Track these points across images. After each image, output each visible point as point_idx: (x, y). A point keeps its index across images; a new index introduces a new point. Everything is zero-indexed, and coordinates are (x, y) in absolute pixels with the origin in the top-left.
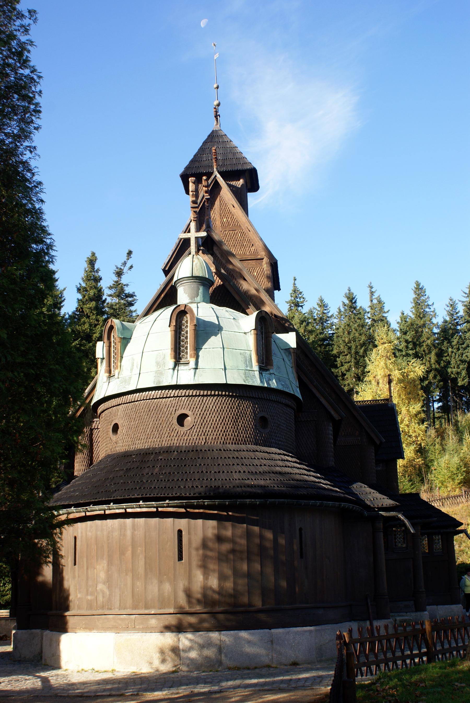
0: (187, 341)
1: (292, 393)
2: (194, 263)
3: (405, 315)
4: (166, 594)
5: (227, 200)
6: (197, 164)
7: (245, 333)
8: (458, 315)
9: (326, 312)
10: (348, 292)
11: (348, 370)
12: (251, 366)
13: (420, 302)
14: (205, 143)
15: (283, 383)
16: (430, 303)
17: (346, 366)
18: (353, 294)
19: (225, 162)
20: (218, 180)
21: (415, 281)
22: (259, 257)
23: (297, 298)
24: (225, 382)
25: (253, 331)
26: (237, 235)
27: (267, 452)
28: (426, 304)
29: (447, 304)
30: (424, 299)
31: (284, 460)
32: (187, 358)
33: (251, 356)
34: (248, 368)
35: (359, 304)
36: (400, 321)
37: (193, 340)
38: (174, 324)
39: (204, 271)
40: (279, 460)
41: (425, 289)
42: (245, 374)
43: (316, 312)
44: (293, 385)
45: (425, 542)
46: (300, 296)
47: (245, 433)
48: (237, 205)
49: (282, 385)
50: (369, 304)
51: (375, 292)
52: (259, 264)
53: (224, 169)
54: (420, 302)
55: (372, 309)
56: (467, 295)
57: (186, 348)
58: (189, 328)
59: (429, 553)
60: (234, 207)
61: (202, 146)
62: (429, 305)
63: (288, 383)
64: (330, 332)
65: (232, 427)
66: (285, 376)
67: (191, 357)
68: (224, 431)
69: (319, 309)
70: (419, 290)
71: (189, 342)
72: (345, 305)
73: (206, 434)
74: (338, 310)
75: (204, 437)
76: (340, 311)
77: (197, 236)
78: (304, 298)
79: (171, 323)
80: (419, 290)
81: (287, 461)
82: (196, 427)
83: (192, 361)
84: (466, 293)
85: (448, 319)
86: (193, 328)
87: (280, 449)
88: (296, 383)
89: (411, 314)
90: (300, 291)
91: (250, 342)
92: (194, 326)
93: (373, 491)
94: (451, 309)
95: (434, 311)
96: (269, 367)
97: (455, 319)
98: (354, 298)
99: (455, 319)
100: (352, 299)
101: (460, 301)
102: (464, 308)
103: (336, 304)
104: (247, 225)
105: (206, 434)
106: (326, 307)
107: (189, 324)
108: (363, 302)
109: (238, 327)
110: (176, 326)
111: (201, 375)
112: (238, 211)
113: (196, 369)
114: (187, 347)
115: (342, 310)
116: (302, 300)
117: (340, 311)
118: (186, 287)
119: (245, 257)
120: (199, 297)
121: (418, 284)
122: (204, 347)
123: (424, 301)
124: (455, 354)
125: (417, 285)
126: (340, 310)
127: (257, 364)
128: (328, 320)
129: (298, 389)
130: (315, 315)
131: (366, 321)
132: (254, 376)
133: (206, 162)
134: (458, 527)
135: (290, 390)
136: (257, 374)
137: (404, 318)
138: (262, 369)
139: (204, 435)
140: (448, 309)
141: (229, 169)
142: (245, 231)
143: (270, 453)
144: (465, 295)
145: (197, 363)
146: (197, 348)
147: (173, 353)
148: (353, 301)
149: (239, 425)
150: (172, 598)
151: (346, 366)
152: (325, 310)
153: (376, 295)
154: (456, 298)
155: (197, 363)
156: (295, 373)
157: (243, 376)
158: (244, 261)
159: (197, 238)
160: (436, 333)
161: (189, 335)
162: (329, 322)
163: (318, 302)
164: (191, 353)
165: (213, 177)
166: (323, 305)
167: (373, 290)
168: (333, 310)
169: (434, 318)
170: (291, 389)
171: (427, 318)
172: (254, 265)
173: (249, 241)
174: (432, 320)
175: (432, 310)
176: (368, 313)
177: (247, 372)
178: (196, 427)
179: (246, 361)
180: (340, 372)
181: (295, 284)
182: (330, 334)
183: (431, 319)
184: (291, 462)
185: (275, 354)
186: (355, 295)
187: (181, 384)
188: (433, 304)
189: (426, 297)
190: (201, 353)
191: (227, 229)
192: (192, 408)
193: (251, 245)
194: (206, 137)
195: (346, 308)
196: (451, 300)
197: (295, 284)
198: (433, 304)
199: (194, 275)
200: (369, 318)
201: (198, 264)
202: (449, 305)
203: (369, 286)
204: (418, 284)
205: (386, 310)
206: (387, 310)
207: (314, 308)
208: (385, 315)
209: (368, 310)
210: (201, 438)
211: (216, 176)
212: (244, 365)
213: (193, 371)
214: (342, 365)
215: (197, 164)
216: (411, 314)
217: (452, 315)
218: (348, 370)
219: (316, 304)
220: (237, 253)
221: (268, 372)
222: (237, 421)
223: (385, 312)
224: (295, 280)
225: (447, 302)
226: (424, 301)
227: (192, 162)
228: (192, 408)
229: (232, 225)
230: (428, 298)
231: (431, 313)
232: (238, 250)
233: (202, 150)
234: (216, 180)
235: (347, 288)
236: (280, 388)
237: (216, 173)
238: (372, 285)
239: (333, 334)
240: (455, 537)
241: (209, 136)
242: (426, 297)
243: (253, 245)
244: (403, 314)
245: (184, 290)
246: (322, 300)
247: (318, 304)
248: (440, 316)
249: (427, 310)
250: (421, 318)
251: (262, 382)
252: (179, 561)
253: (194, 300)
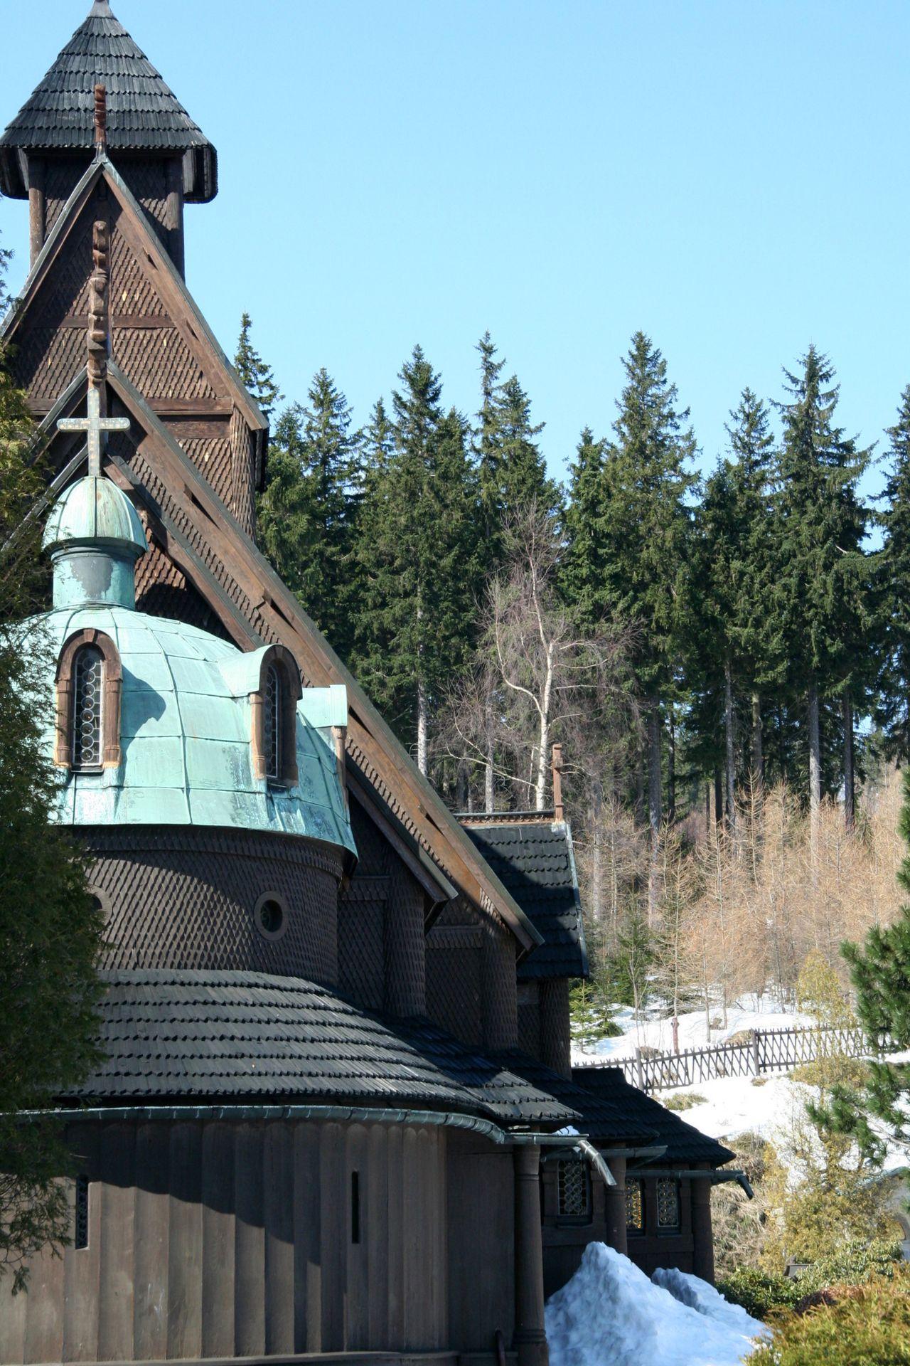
0: (98, 719)
1: (338, 842)
2: (100, 504)
3: (594, 442)
4: (46, 1327)
5: (130, 236)
6: (42, 122)
7: (233, 698)
8: (769, 449)
9: (336, 422)
10: (412, 361)
11: (402, 621)
12: (249, 782)
13: (644, 411)
14: (66, 54)
15: (319, 821)
16: (678, 408)
17: (398, 607)
18: (429, 369)
19: (127, 122)
20: (108, 179)
21: (632, 334)
22: (218, 410)
23: (252, 386)
24: (188, 822)
25: (253, 697)
26: (159, 343)
27: (279, 988)
28: (665, 411)
29: (736, 408)
30: (660, 393)
31: (320, 1008)
32: (96, 759)
33: (247, 757)
34: (242, 787)
35: (444, 405)
36: (576, 461)
37: (112, 716)
38: (68, 676)
39: (125, 527)
40: (308, 1007)
41: (665, 362)
42: (234, 800)
43: (307, 420)
44: (339, 820)
45: (636, 1201)
46: (261, 378)
47: (229, 942)
48: (160, 257)
49: (317, 825)
50: (478, 403)
51: (499, 366)
52: (219, 428)
53: (126, 142)
54: (644, 411)
55: (487, 422)
56: (798, 388)
57: (96, 734)
58: (102, 686)
59: (643, 1231)
60: (150, 260)
61: (57, 64)
62: (671, 415)
63: (329, 818)
64: (347, 491)
65: (199, 928)
66: (323, 801)
67: (108, 757)
68: (182, 938)
69: (316, 413)
70: (644, 361)
71: (101, 721)
72: (404, 405)
73: (139, 944)
74: (375, 414)
75: (134, 952)
76: (381, 418)
77: (103, 426)
78: (272, 388)
79: (62, 675)
80: (644, 361)
81: (326, 1008)
82: (116, 926)
83: (111, 769)
84: (795, 381)
85: (734, 461)
86: (114, 687)
87: (307, 979)
88: (344, 814)
89: (614, 439)
90: (262, 363)
91: (245, 722)
92: (115, 684)
93: (519, 1080)
94: (746, 426)
95: (689, 437)
96: (289, 782)
97: (757, 463)
98: (433, 383)
99: (757, 463)
100: (422, 382)
101: (776, 404)
102: (786, 427)
103: (370, 393)
104: (179, 298)
105: (139, 944)
106: (340, 407)
107: (102, 677)
108: (461, 397)
109: (217, 681)
110: (71, 681)
111: (133, 802)
112: (162, 273)
113: (119, 787)
114: (97, 733)
115: (393, 417)
116: (266, 392)
117: (381, 418)
118: (79, 562)
119: (179, 409)
120: (111, 590)
121: (642, 344)
122: (138, 734)
123: (658, 402)
124: (752, 578)
125: (638, 349)
126: (381, 411)
127: (261, 776)
128: (340, 453)
129: (349, 830)
130: (302, 433)
131: (467, 459)
132: (255, 805)
133: (71, 117)
134: (721, 1165)
135: (334, 838)
136: (261, 800)
137: (589, 452)
138: (274, 788)
139: (135, 946)
140: (735, 426)
141: (139, 142)
142: (183, 333)
143: (286, 990)
144: (792, 386)
145: (121, 774)
146: (122, 738)
147: (64, 747)
148: (430, 395)
149: (215, 923)
150: (59, 1335)
151: (398, 607)
152: (335, 416)
153: (503, 377)
154: (762, 395)
155: (121, 774)
156: (342, 788)
157: (230, 806)
158: (181, 425)
159: (102, 433)
160: (689, 510)
161: (101, 703)
162: (345, 458)
163: (313, 388)
164: (108, 747)
165: (93, 168)
166: (326, 398)
167: (494, 359)
168: (359, 419)
169: (687, 460)
170: (336, 834)
171: (666, 458)
172: (202, 431)
173: (192, 362)
174: (681, 464)
175: (683, 431)
176: (476, 433)
177: (239, 795)
178: (116, 926)
179: (236, 768)
180: (375, 626)
181: (244, 338)
182: (347, 497)
183: (676, 462)
184: (335, 1010)
185: (301, 747)
186: (434, 374)
187: (85, 823)
188: (687, 413)
189: (667, 388)
190: (130, 752)
191: (131, 324)
192: (106, 883)
193: (197, 374)
194: (67, 38)
195: (406, 415)
196: (748, 399)
197: (244, 338)
198: (687, 413)
199: (99, 534)
200: (478, 452)
201: (110, 505)
202: (741, 416)
203: (482, 345)
204: (642, 344)
205: (533, 423)
206: (538, 424)
207: (299, 409)
208: (532, 440)
209: (477, 423)
210: (127, 953)
211: (102, 167)
212: (231, 778)
213: (112, 793)
214: (384, 605)
215: (42, 122)
216: (614, 439)
217: (747, 447)
218: (402, 621)
219: (307, 393)
220: (157, 395)
221: (285, 795)
222: (212, 914)
223: (531, 432)
224: (247, 324)
225: (736, 402)
226: (658, 402)
227: (29, 110)
228: (106, 883)
229: (143, 312)
230: (674, 390)
231: (681, 443)
232: (161, 386)
233: (57, 78)
234: (102, 177)
235: (413, 350)
236: (313, 833)
237: (102, 159)
238: (490, 343)
239: (358, 497)
240: (713, 1188)
241: (79, 33)
242: (667, 388)
243: (201, 374)
244: (587, 439)
245: (74, 569)
246: (325, 385)
247: (312, 396)
248: (709, 451)
249: (667, 430)
250: (647, 458)
251: (271, 819)
252: (77, 1247)
253: (100, 598)
